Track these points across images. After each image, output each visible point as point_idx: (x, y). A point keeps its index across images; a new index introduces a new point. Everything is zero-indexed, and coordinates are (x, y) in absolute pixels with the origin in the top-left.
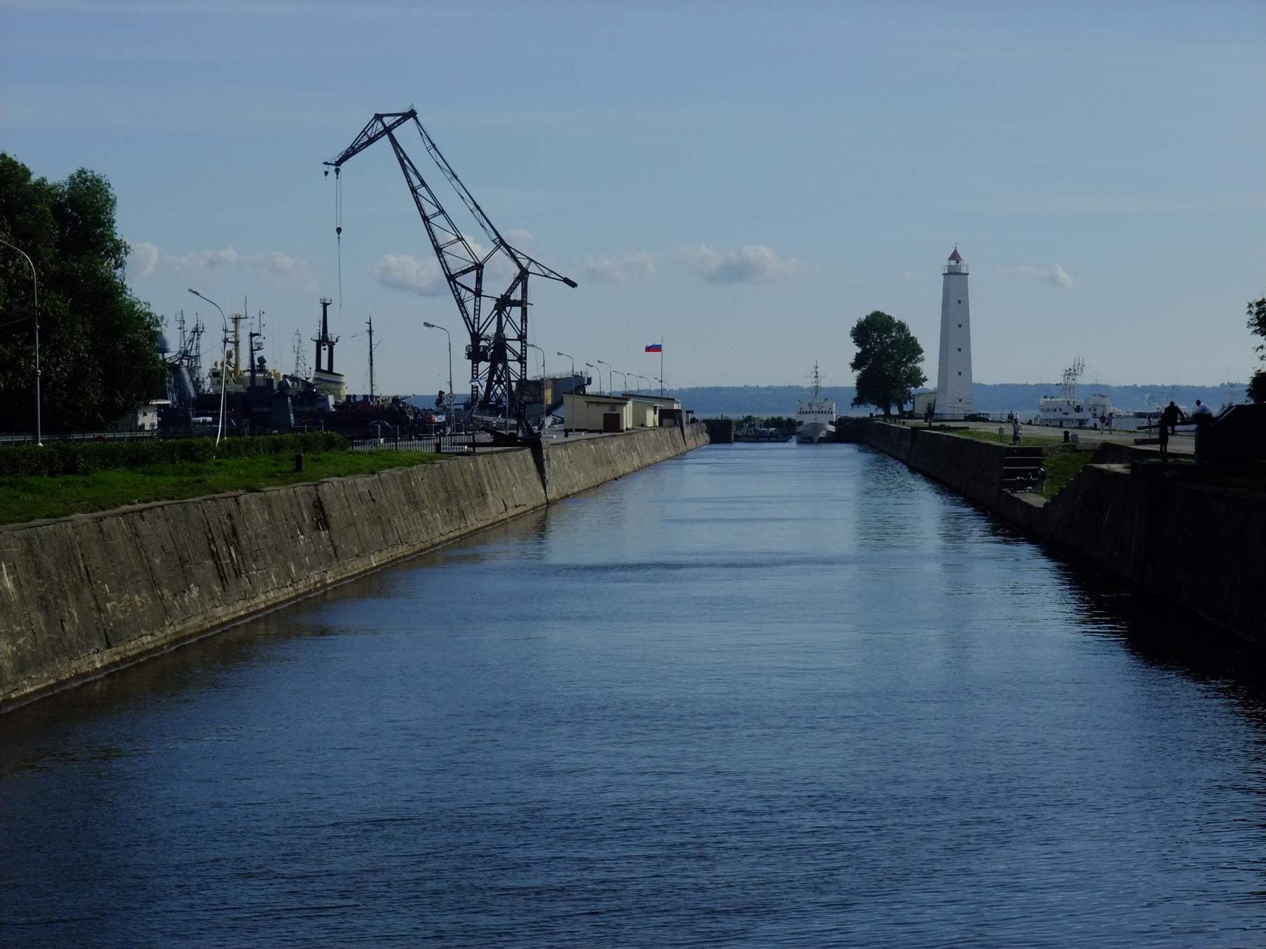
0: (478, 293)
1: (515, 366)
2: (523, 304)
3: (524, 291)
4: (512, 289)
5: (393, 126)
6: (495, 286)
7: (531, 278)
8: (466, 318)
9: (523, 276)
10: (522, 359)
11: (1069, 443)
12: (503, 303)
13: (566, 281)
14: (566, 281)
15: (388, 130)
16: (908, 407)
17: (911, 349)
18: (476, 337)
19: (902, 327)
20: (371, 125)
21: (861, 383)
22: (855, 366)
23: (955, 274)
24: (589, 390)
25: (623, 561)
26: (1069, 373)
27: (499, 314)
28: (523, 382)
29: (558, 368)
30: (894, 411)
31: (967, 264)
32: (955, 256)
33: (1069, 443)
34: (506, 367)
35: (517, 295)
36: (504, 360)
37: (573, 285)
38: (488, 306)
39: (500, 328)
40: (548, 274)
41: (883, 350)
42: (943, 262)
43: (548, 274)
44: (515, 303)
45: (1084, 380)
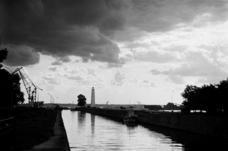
0: (30, 91)
1: (34, 100)
2: (36, 92)
3: (36, 90)
4: (34, 90)
5: (20, 69)
6: (32, 89)
7: (37, 89)
8: (28, 94)
9: (36, 89)
10: (35, 99)
11: (176, 105)
12: (33, 92)
13: (41, 90)
14: (41, 90)
15: (19, 70)
16: (84, 106)
17: (85, 99)
18: (29, 96)
19: (84, 96)
20: (16, 69)
21: (79, 103)
22: (78, 101)
23: (93, 90)
24: (44, 103)
25: (73, 147)
26: (107, 102)
27: (33, 94)
28: (35, 102)
29: (40, 100)
30: (82, 107)
31: (95, 89)
32: (93, 88)
33: (176, 105)
34: (33, 100)
35: (35, 91)
36: (33, 99)
37: (42, 90)
38: (31, 92)
39: (33, 95)
40: (39, 89)
41: (82, 99)
42: (92, 88)
43: (39, 89)
44: (34, 92)
45: (109, 104)
